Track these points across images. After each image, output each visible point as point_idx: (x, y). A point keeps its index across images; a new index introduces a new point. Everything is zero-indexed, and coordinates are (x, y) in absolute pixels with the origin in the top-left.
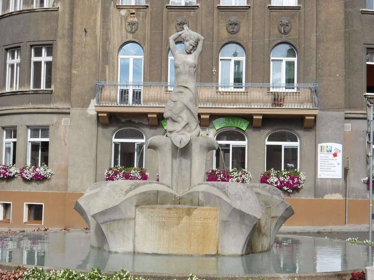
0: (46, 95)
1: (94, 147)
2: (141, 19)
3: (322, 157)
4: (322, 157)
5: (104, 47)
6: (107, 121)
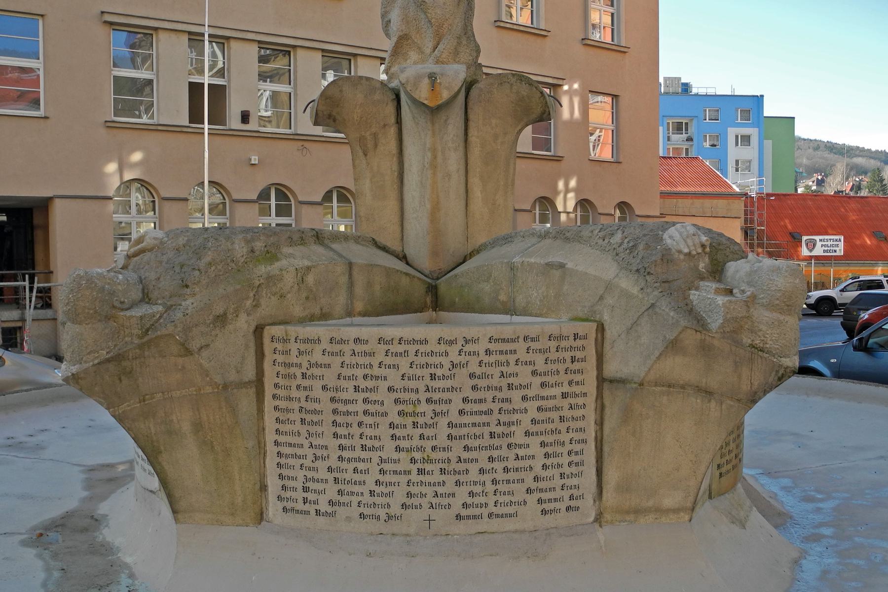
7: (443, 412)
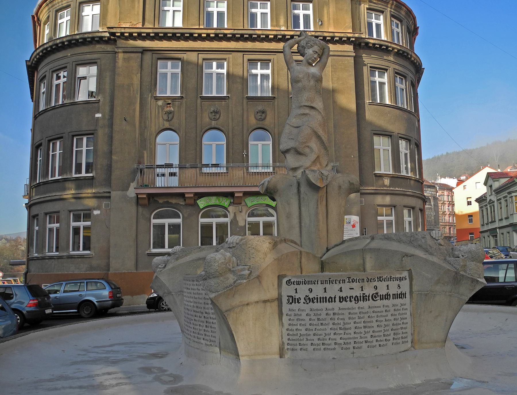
0: (84, 181)
1: (135, 227)
2: (176, 108)
5: (142, 134)
6: (146, 202)
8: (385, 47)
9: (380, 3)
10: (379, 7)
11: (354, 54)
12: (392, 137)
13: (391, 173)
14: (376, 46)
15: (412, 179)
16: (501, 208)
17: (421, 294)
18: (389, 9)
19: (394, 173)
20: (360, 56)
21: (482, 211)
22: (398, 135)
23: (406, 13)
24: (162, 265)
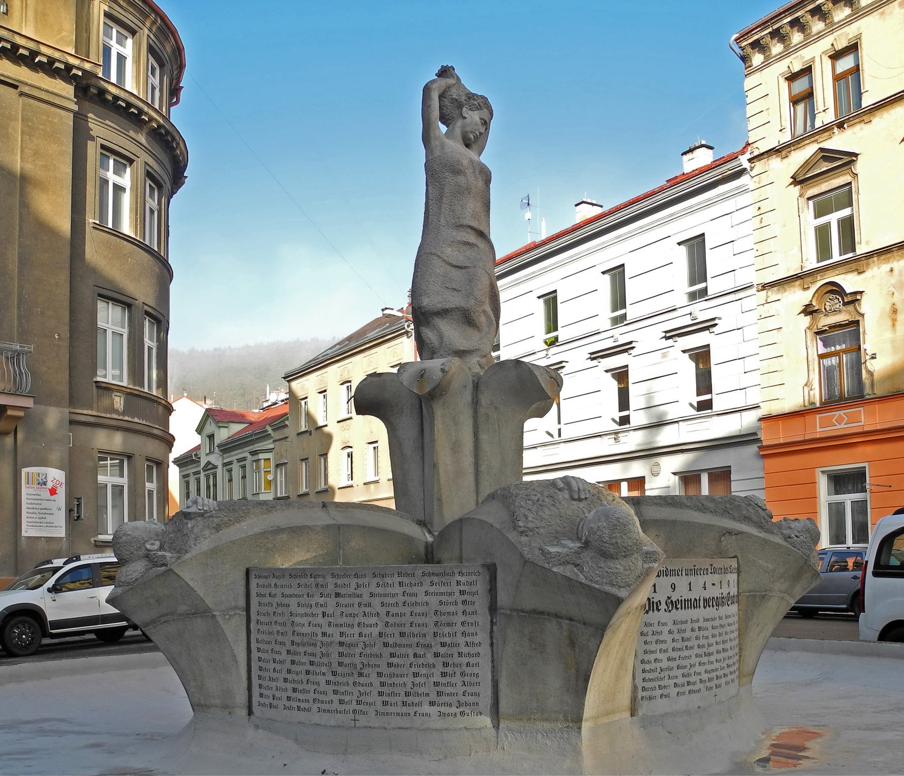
3: (29, 495)
4: (29, 495)
7: (401, 683)
8: (136, 112)
9: (131, 10)
10: (130, 18)
11: (75, 108)
12: (133, 309)
13: (125, 384)
14: (120, 102)
15: (159, 403)
16: (230, 480)
17: (754, 596)
18: (146, 31)
19: (131, 386)
20: (84, 116)
21: (188, 483)
22: (143, 307)
23: (173, 51)
24: (153, 544)
